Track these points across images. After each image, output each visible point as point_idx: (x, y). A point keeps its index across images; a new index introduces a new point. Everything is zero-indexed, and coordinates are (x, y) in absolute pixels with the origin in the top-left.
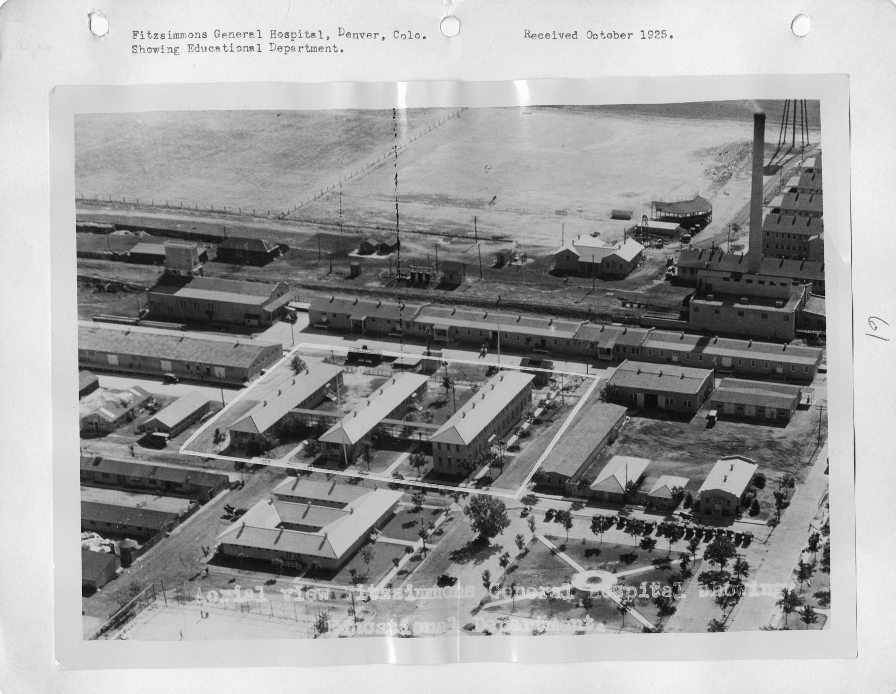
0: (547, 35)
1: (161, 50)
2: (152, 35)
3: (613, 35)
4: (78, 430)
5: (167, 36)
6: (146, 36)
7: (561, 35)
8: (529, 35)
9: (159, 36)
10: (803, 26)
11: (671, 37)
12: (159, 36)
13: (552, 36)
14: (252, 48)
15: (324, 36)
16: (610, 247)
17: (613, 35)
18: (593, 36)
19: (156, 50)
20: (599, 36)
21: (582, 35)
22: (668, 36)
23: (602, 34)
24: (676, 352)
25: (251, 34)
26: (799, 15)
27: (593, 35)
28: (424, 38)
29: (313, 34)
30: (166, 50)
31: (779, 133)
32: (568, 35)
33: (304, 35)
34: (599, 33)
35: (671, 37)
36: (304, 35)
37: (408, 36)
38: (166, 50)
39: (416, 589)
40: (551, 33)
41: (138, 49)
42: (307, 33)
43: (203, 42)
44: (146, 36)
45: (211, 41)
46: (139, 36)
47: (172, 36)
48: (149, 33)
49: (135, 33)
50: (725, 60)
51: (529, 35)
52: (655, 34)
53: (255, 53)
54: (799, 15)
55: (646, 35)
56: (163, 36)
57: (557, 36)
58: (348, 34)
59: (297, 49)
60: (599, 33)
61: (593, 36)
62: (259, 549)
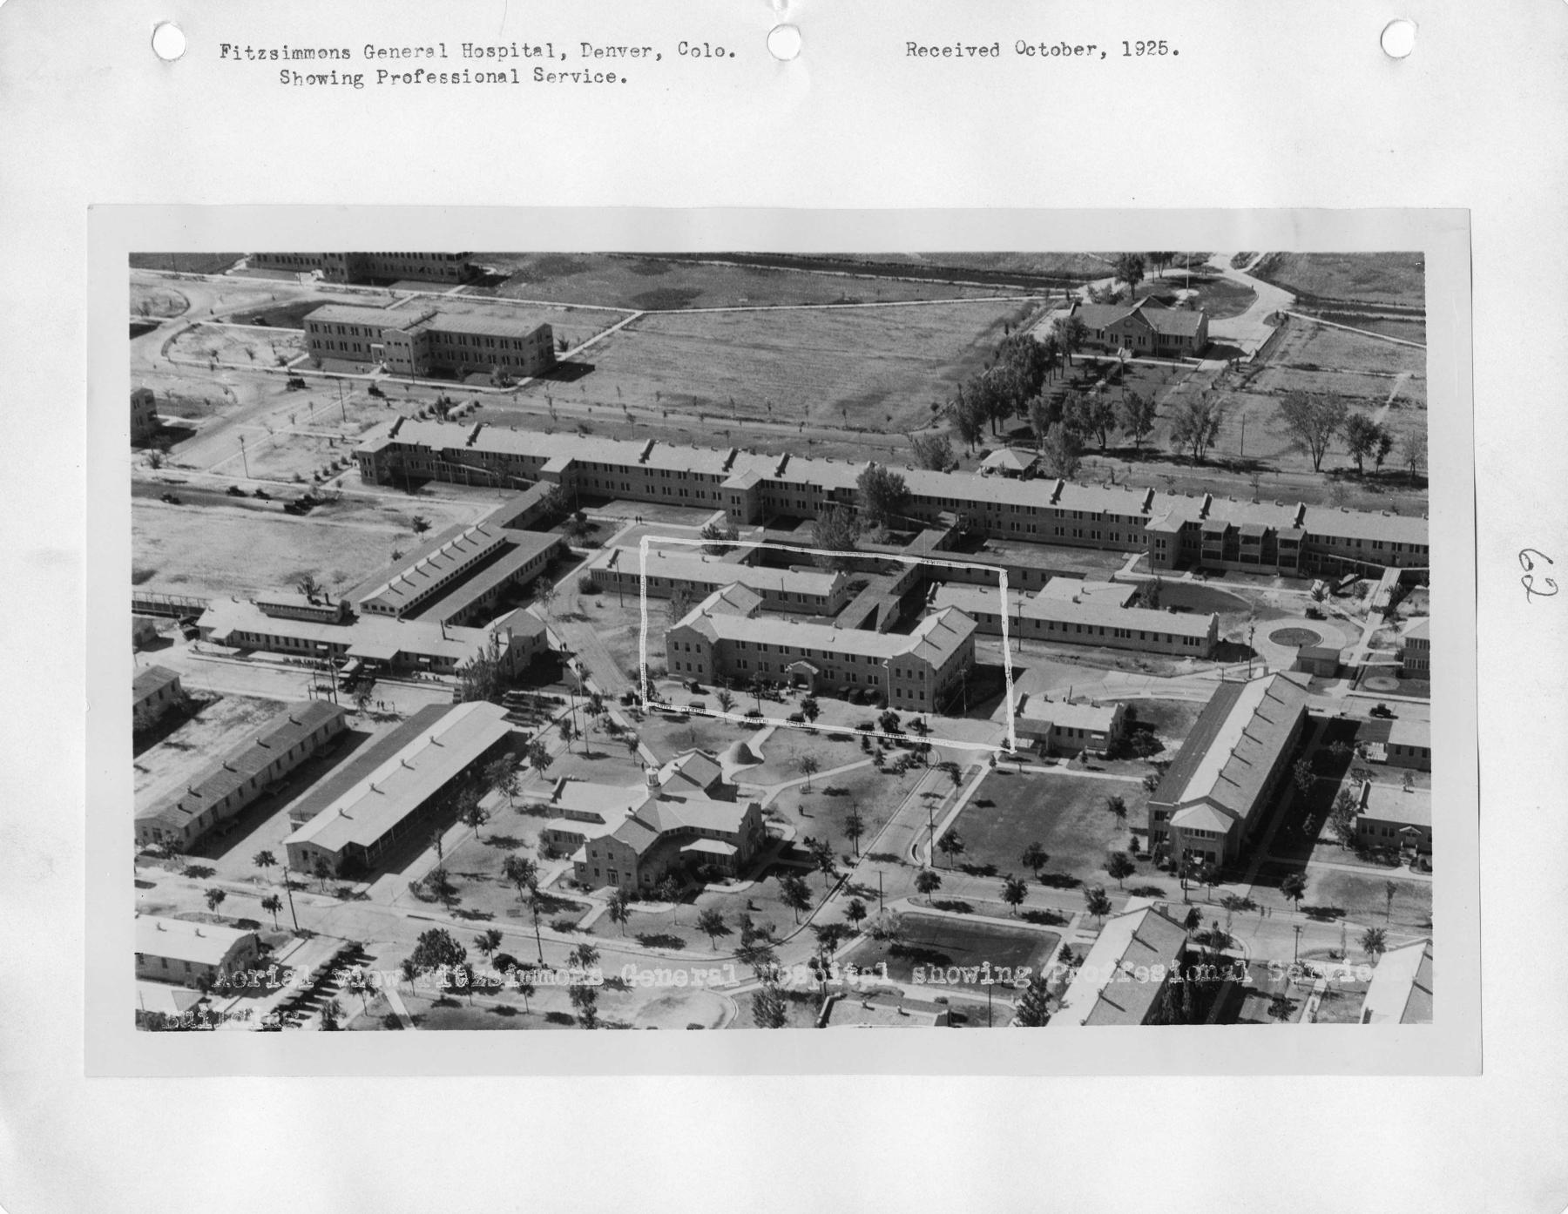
0: (947, 50)
1: (330, 80)
3: (1061, 50)
4: (128, 439)
5: (281, 54)
7: (971, 50)
8: (914, 49)
9: (267, 54)
11: (1176, 53)
14: (502, 76)
15: (557, 53)
17: (1061, 50)
18: (1027, 50)
19: (322, 79)
20: (1038, 51)
21: (1007, 48)
23: (1043, 47)
24: (806, 654)
25: (431, 51)
26: (163, 23)
28: (1176, 53)
29: (537, 50)
31: (1421, 255)
32: (983, 50)
33: (520, 51)
35: (564, 57)
36: (520, 51)
37: (704, 52)
38: (339, 79)
39: (997, 969)
40: (953, 46)
41: (292, 76)
43: (434, 65)
44: (243, 54)
45: (456, 63)
48: (526, 48)
49: (225, 48)
50: (263, 1094)
51: (914, 49)
53: (508, 86)
54: (163, 23)
55: (1132, 50)
57: (965, 52)
58: (598, 52)
61: (1027, 50)
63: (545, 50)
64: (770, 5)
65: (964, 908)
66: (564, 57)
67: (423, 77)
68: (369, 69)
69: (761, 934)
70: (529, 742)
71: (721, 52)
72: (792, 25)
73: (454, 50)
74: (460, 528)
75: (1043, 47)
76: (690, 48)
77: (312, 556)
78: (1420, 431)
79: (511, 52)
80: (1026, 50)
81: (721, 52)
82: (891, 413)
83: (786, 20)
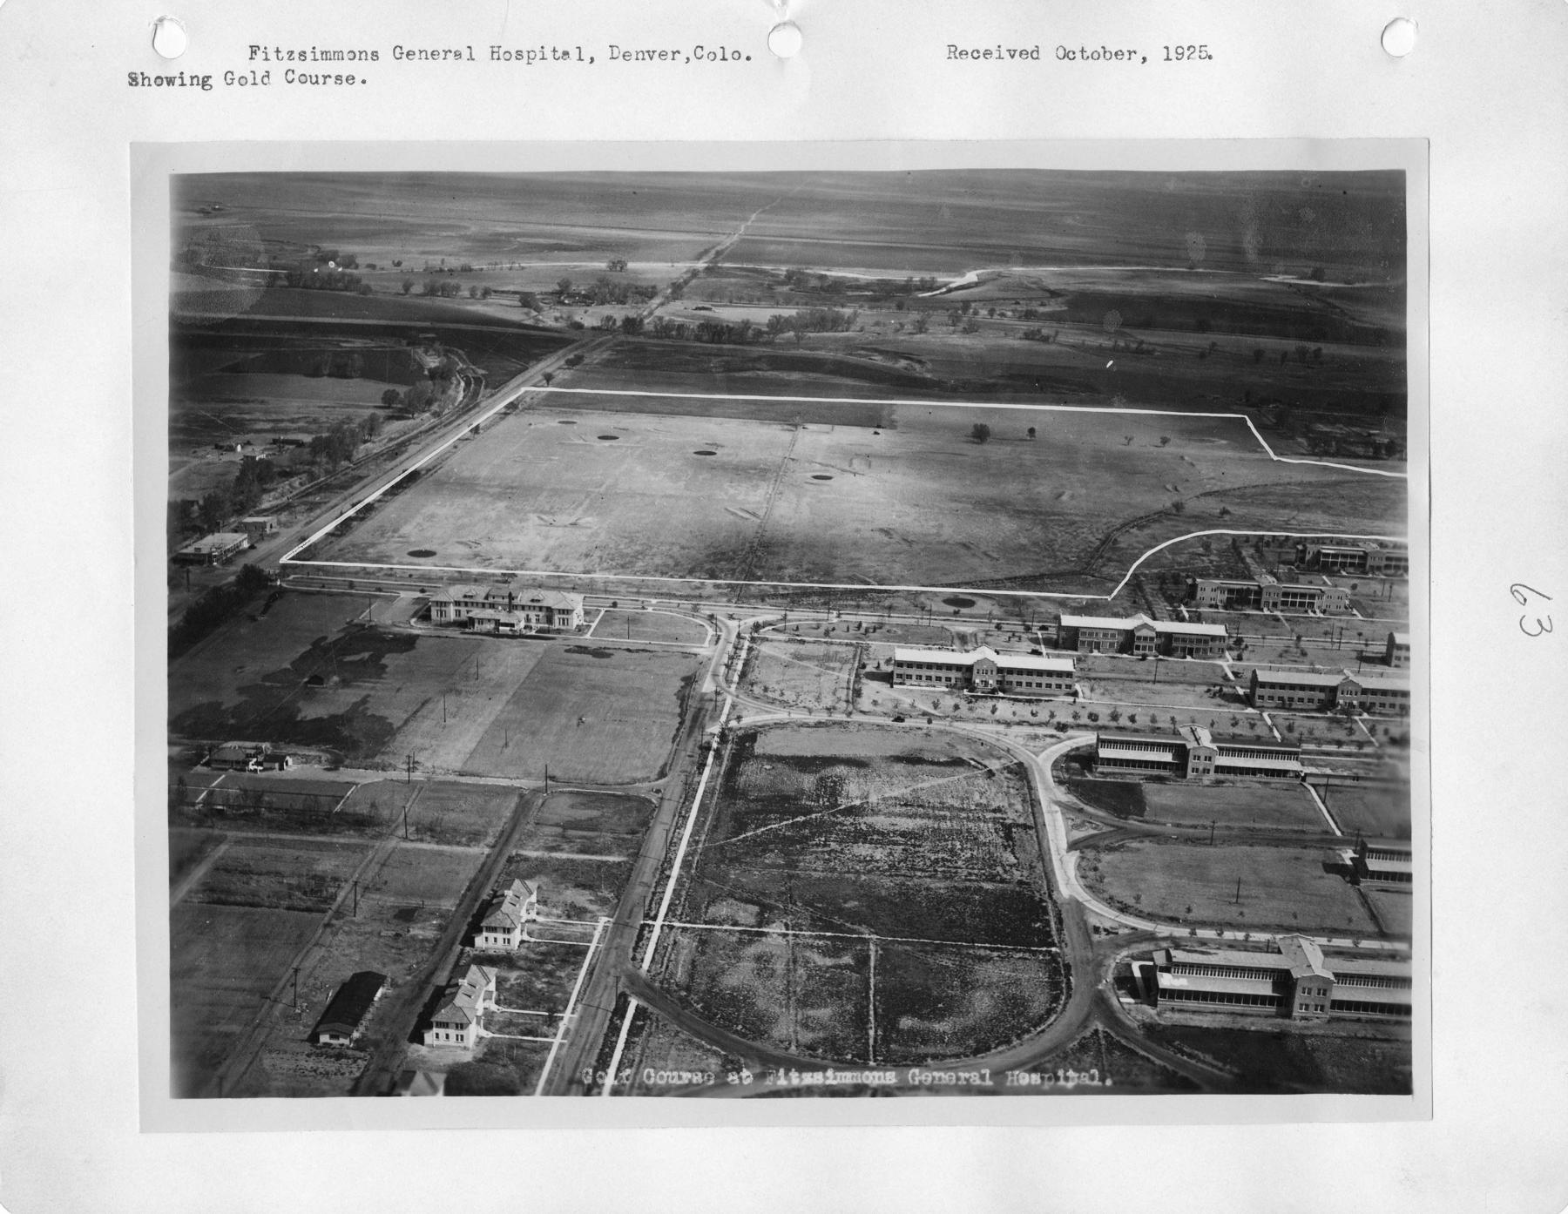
0: (987, 53)
1: (178, 81)
2: (284, 54)
5: (310, 56)
6: (272, 55)
8: (956, 52)
9: (296, 55)
10: (1403, 39)
12: (296, 55)
13: (996, 54)
16: (881, 319)
19: (170, 81)
20: (1078, 55)
21: (1047, 54)
22: (744, 57)
26: (161, 20)
27: (1066, 55)
29: (566, 53)
30: (187, 81)
33: (549, 54)
35: (592, 60)
36: (549, 54)
37: (720, 56)
38: (187, 81)
40: (309, 50)
44: (272, 55)
46: (260, 55)
47: (318, 56)
48: (278, 51)
49: (254, 50)
51: (956, 52)
52: (1187, 53)
54: (161, 20)
55: (1173, 55)
56: (303, 54)
57: (1006, 55)
59: (321, 80)
62: (170, 676)
64: (772, 5)
66: (592, 60)
67: (330, 81)
68: (278, 68)
69: (1400, 647)
70: (782, 1071)
71: (737, 55)
72: (793, 24)
76: (705, 53)
80: (1066, 55)
81: (737, 55)
82: (1194, 907)
83: (786, 19)
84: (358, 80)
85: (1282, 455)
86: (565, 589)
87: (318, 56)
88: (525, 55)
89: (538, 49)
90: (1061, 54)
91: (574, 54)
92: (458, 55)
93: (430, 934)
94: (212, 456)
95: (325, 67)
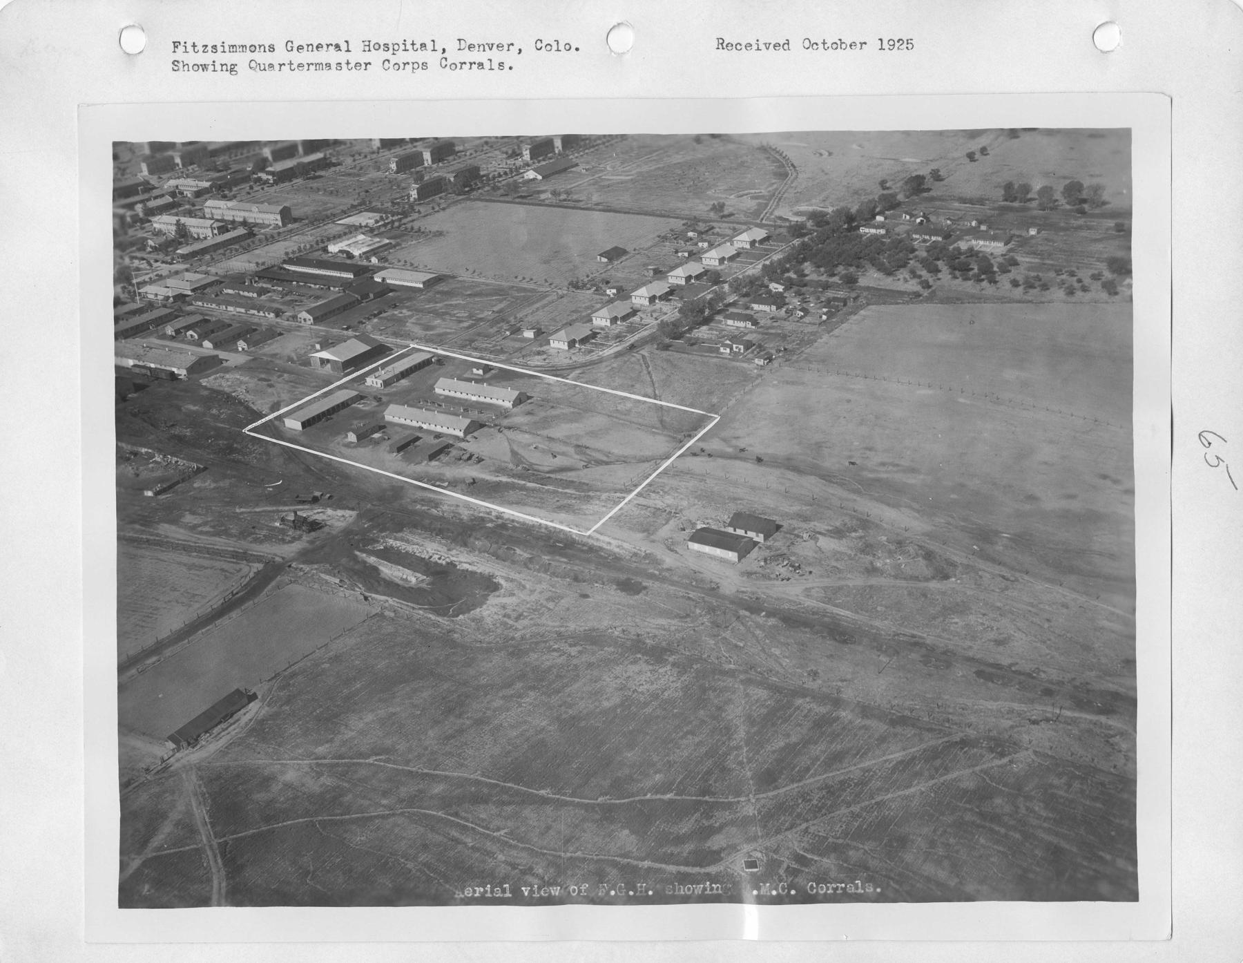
1: (211, 68)
3: (839, 44)
5: (220, 49)
6: (190, 49)
7: (767, 46)
8: (722, 44)
9: (209, 48)
12: (209, 48)
15: (439, 47)
17: (839, 44)
18: (813, 45)
19: (205, 67)
20: (821, 46)
21: (796, 44)
28: (577, 49)
29: (423, 45)
30: (218, 67)
33: (409, 47)
34: (820, 42)
36: (409, 47)
37: (555, 47)
38: (218, 67)
40: (753, 42)
41: (181, 65)
42: (194, 46)
44: (190, 49)
46: (181, 48)
47: (227, 49)
48: (194, 46)
49: (176, 44)
51: (722, 44)
52: (897, 45)
55: (886, 46)
57: (762, 47)
59: (277, 67)
60: (820, 42)
63: (430, 46)
65: (190, 567)
71: (568, 47)
73: (357, 46)
74: (786, 721)
75: (824, 43)
77: (557, 624)
78: (1013, 618)
79: (402, 47)
81: (568, 47)
84: (506, 66)
85: (299, 164)
86: (211, 284)
87: (227, 49)
88: (391, 47)
89: (401, 43)
90: (807, 44)
91: (430, 46)
92: (337, 47)
93: (355, 422)
94: (768, 263)
95: (483, 54)
